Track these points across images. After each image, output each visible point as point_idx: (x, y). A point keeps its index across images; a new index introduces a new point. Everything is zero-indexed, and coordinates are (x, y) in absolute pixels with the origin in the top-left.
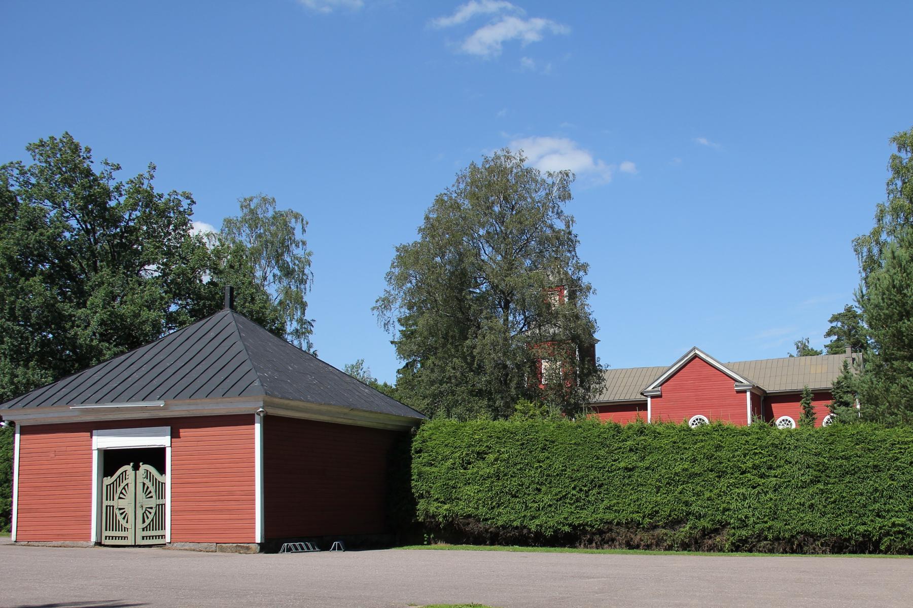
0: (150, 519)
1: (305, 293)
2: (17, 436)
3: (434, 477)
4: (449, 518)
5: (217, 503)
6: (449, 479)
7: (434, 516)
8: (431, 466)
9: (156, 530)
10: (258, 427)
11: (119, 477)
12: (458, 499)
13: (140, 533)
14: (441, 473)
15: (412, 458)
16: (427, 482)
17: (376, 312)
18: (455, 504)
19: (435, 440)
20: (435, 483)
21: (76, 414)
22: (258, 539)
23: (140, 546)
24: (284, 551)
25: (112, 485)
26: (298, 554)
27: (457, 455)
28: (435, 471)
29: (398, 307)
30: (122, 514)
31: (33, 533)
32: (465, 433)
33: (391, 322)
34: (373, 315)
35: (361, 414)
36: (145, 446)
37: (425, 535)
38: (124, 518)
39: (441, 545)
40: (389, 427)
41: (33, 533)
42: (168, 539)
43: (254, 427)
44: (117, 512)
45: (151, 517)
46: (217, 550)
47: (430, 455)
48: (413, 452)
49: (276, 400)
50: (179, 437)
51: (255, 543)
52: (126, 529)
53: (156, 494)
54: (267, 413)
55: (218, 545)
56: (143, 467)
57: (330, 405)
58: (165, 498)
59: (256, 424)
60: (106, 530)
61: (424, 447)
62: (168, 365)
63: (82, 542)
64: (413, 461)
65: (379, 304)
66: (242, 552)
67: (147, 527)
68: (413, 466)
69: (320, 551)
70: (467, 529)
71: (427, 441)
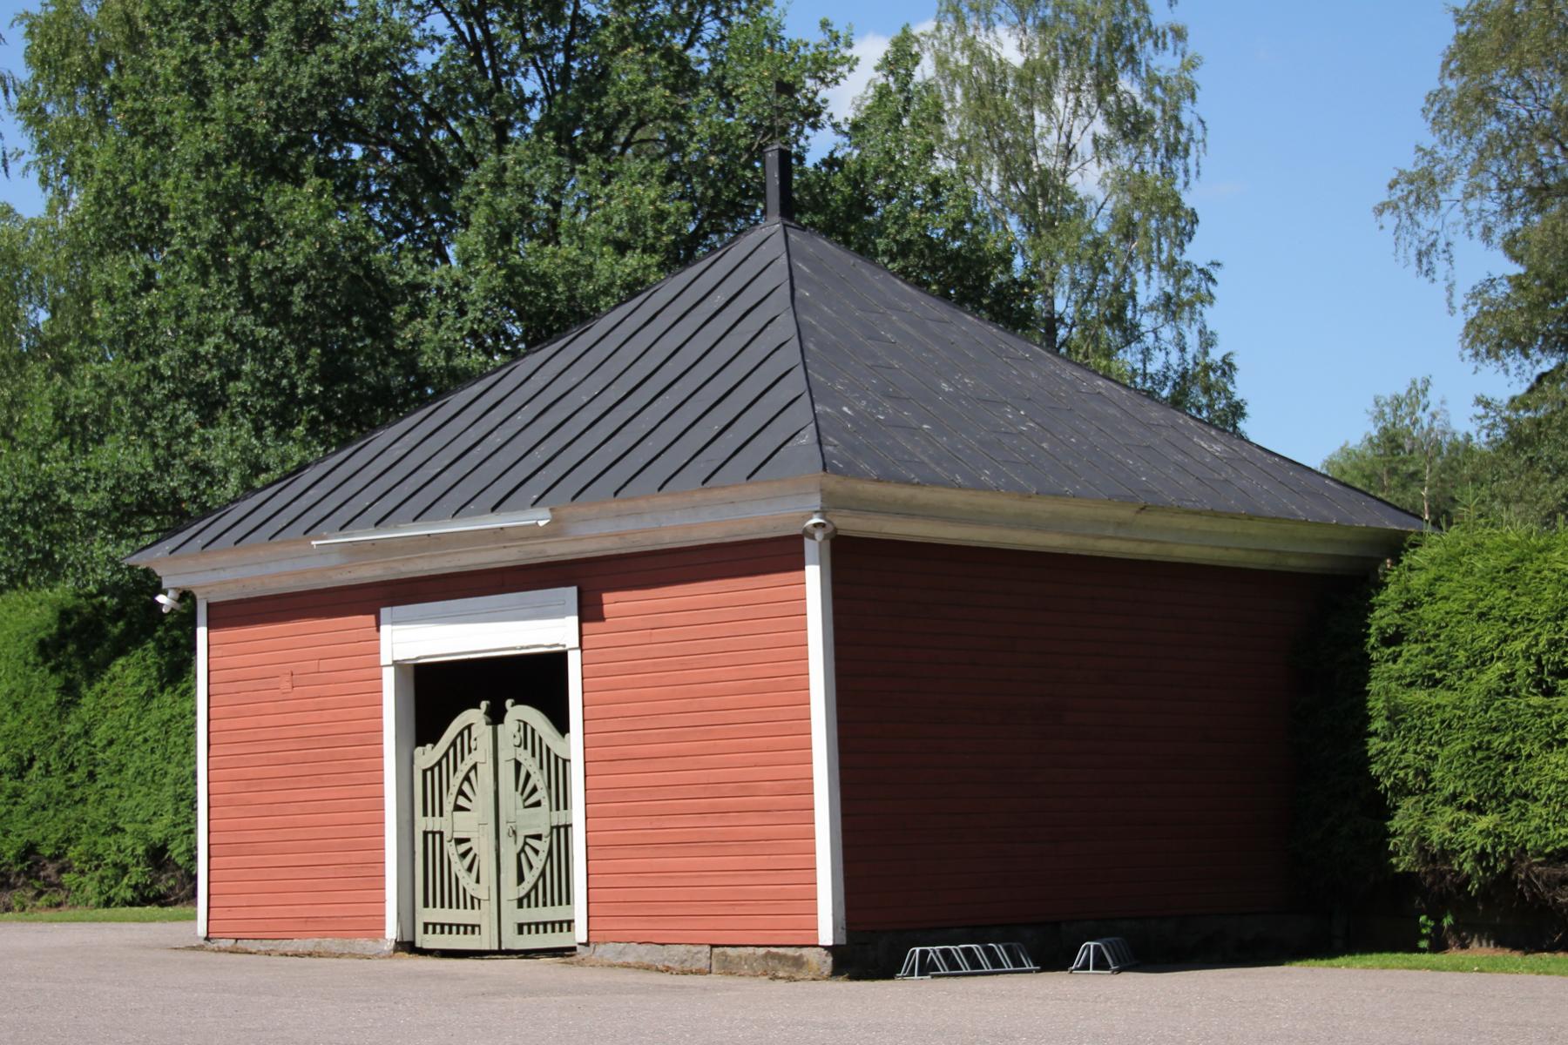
0: (536, 872)
1: (1186, 184)
2: (202, 632)
3: (1443, 722)
4: (1496, 860)
5: (711, 820)
6: (1495, 730)
7: (1446, 854)
8: (1434, 686)
9: (553, 904)
10: (813, 576)
11: (454, 744)
12: (1525, 796)
13: (512, 915)
14: (1465, 709)
15: (1372, 661)
16: (1418, 741)
17: (1389, 219)
18: (1514, 812)
19: (1446, 598)
20: (1447, 744)
21: (334, 560)
22: (826, 936)
23: (509, 953)
24: (912, 973)
25: (436, 770)
26: (1001, 977)
27: (1519, 645)
28: (1443, 703)
29: (1460, 197)
30: (464, 855)
31: (245, 912)
32: (1546, 572)
33: (1441, 245)
34: (1382, 227)
35: (1185, 522)
36: (515, 649)
37: (1423, 918)
38: (470, 869)
39: (1480, 952)
40: (1293, 563)
41: (245, 912)
42: (580, 933)
43: (804, 577)
44: (451, 850)
45: (538, 862)
46: (714, 970)
47: (1430, 651)
48: (1372, 640)
49: (869, 489)
50: (600, 617)
51: (817, 946)
52: (476, 901)
53: (549, 786)
54: (836, 530)
55: (716, 950)
56: (517, 713)
57: (1058, 495)
58: (566, 808)
59: (807, 568)
60: (426, 905)
61: (1410, 625)
62: (585, 399)
63: (362, 941)
64: (1375, 671)
65: (1398, 193)
66: (781, 974)
67: (528, 895)
68: (1373, 686)
69: (1038, 971)
70: (1560, 900)
71: (1421, 604)
